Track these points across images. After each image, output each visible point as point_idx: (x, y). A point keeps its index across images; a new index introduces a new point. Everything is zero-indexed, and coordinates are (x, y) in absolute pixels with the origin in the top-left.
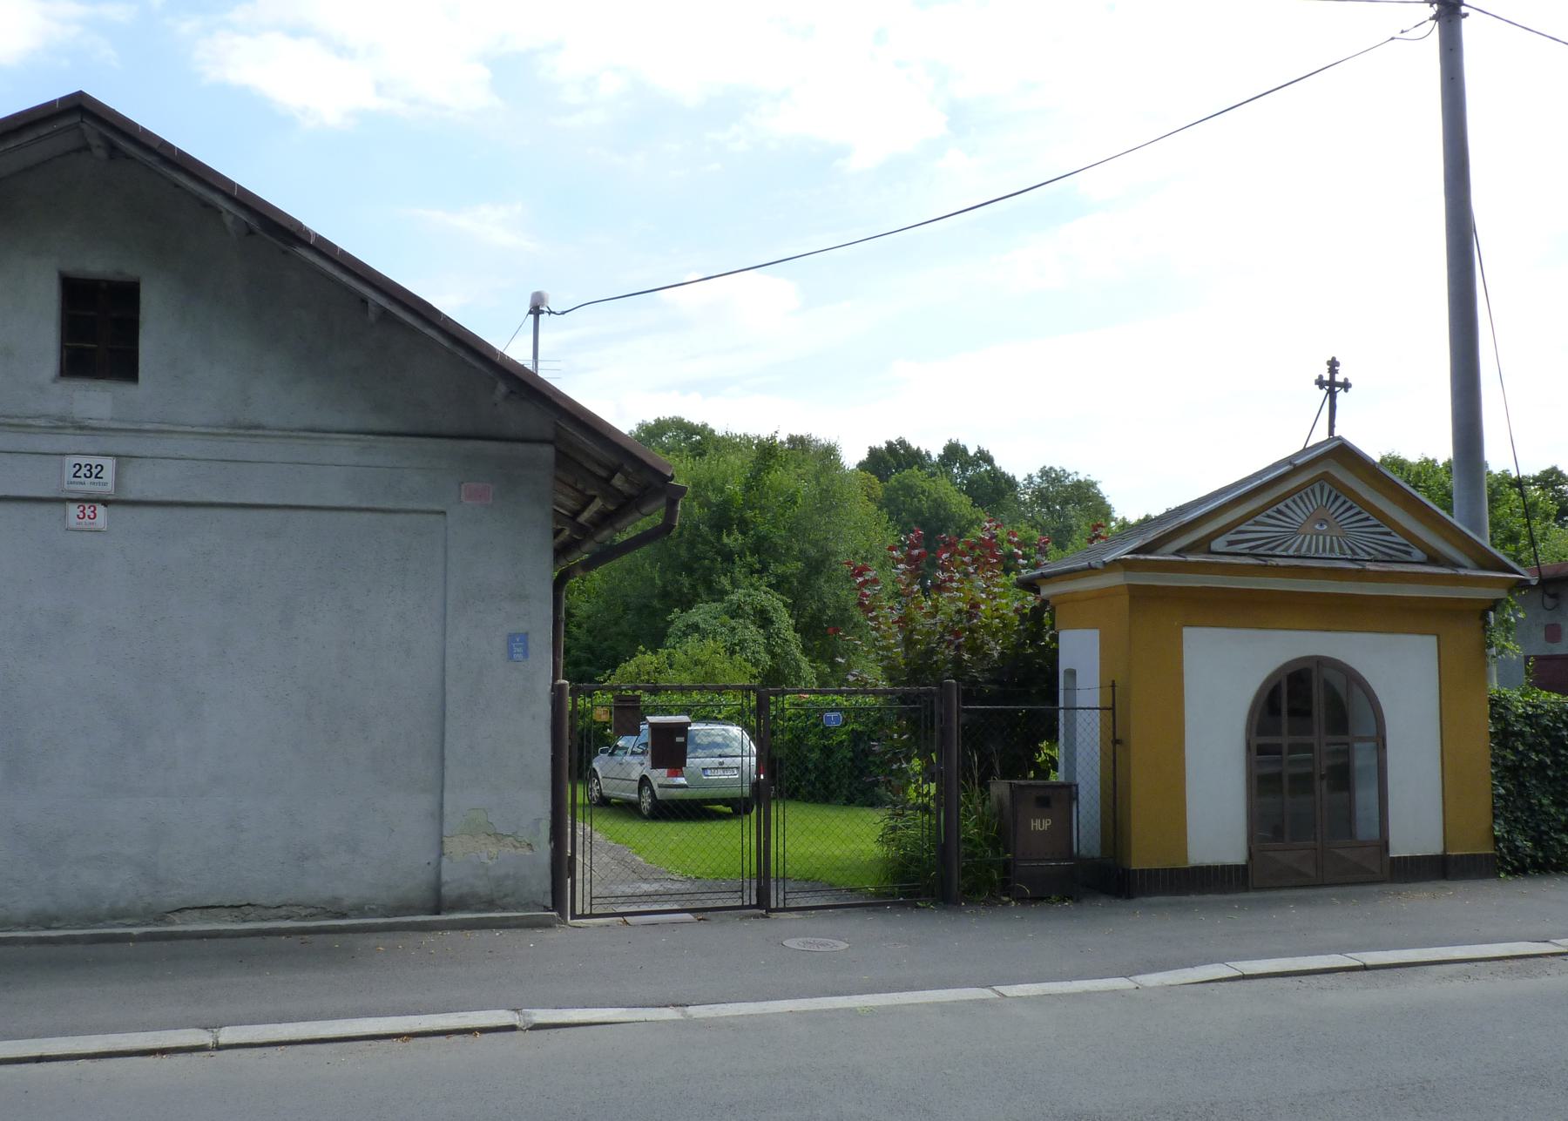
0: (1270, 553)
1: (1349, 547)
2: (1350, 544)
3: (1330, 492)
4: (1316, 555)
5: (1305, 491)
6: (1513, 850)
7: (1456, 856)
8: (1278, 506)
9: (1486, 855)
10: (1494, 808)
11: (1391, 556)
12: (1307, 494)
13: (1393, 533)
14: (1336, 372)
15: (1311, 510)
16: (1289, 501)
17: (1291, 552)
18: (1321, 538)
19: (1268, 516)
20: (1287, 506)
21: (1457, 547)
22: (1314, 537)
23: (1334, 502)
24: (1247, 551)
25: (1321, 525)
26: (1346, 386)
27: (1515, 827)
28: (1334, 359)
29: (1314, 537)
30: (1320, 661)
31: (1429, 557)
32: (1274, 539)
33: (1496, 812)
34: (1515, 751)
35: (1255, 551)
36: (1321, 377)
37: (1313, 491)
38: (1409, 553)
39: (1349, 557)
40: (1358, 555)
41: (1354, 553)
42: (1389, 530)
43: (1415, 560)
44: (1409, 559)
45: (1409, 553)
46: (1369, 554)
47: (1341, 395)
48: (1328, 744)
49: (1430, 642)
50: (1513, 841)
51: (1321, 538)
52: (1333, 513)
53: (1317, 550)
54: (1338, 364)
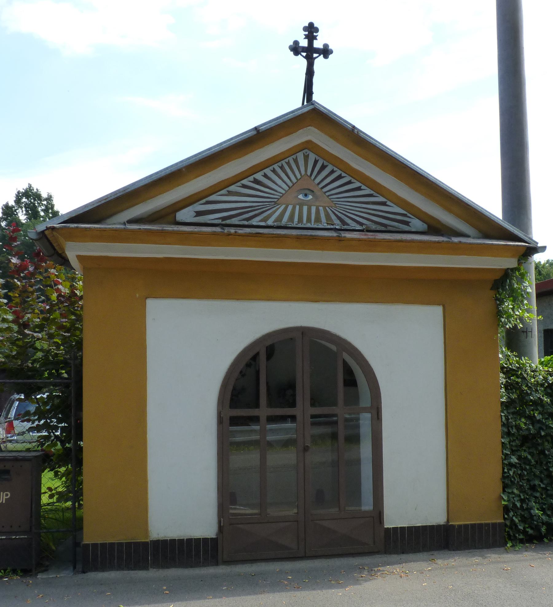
0: (246, 223)
1: (339, 218)
2: (337, 212)
3: (316, 162)
4: (300, 225)
5: (287, 160)
6: (528, 519)
7: (460, 526)
8: (255, 176)
9: (494, 525)
10: (504, 477)
11: (385, 225)
12: (288, 164)
13: (389, 203)
14: (315, 38)
15: (294, 180)
16: (268, 171)
17: (270, 222)
18: (305, 208)
19: (244, 186)
20: (265, 176)
21: (458, 216)
22: (298, 207)
23: (319, 172)
24: (219, 221)
25: (306, 195)
26: (326, 52)
27: (531, 495)
28: (311, 25)
29: (298, 207)
30: (304, 331)
31: (429, 227)
32: (252, 209)
33: (506, 481)
34: (531, 418)
35: (228, 222)
36: (296, 43)
37: (296, 161)
38: (407, 223)
39: (337, 227)
40: (348, 225)
41: (343, 222)
42: (372, 192)
43: (413, 230)
44: (406, 228)
45: (407, 223)
46: (361, 224)
47: (319, 62)
48: (313, 417)
49: (437, 311)
50: (529, 509)
51: (305, 208)
52: (319, 184)
53: (300, 220)
54: (317, 30)
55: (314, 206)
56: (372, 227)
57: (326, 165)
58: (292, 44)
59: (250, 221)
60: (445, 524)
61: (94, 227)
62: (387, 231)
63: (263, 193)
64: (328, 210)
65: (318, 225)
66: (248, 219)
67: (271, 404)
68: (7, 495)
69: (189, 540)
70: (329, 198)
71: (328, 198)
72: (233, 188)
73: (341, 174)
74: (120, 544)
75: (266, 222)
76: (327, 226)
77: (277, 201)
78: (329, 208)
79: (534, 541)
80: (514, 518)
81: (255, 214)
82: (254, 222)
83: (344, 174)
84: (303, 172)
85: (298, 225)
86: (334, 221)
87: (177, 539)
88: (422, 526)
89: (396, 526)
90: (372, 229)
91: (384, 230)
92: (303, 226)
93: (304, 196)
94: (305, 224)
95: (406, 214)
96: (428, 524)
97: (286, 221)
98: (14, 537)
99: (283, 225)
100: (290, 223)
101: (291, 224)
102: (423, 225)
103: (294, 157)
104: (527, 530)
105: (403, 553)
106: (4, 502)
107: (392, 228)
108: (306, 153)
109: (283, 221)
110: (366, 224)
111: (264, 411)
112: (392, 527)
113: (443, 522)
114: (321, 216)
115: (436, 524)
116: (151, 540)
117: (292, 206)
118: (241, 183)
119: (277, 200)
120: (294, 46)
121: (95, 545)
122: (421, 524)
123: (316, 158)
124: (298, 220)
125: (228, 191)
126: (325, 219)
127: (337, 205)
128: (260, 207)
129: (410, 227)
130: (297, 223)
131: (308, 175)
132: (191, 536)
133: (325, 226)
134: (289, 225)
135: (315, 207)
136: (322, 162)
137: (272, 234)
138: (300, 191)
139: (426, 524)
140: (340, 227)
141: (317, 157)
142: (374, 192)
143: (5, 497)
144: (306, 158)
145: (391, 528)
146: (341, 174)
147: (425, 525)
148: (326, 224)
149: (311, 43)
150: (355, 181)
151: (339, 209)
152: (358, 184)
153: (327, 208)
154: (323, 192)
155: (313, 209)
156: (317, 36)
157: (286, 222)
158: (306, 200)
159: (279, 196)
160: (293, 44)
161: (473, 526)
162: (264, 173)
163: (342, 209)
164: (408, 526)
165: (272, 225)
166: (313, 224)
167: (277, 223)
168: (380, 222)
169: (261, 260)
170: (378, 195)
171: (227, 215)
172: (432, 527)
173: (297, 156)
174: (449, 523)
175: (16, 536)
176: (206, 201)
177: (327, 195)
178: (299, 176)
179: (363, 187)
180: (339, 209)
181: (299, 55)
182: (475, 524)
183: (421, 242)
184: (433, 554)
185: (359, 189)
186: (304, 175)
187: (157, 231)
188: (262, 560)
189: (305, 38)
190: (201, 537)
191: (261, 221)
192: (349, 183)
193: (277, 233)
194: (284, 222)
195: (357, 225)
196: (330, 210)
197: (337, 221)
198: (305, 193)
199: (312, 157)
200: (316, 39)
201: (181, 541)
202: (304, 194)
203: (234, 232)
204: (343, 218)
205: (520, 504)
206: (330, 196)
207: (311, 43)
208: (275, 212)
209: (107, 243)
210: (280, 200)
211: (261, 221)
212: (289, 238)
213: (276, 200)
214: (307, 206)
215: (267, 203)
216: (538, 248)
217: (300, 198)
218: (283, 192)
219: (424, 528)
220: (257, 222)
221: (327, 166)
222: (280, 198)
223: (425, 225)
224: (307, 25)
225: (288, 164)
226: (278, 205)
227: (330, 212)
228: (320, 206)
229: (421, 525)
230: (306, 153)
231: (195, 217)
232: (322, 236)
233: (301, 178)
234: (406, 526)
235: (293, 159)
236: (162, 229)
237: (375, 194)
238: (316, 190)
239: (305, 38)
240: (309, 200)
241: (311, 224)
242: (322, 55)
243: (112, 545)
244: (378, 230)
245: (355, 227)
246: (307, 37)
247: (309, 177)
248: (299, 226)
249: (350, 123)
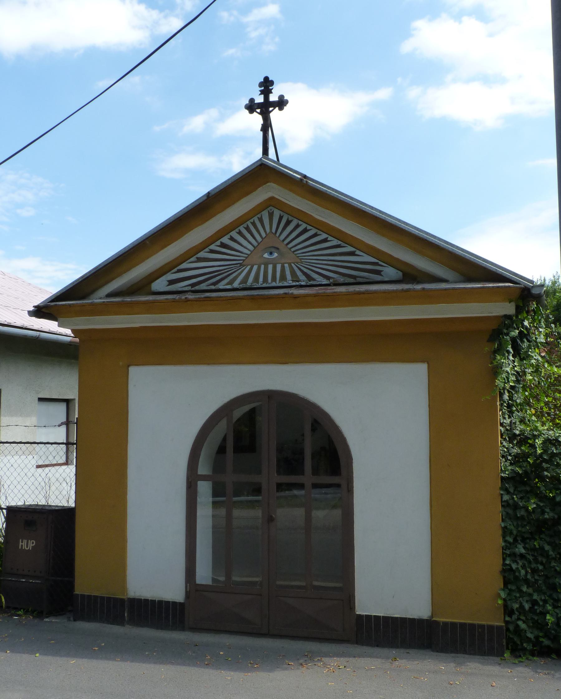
0: (213, 287)
3: (281, 218)
4: (265, 285)
5: (252, 220)
7: (446, 624)
9: (491, 627)
10: (503, 571)
11: (354, 277)
12: (254, 224)
13: (358, 252)
15: (259, 239)
16: (234, 234)
17: (236, 285)
18: (270, 267)
19: (212, 251)
20: (232, 239)
22: (263, 267)
25: (271, 253)
28: (266, 79)
29: (263, 267)
31: (405, 274)
35: (197, 288)
36: (252, 100)
37: (261, 220)
38: (378, 273)
39: (303, 283)
40: (314, 280)
42: (340, 242)
43: (386, 279)
45: (378, 273)
46: (328, 278)
47: (275, 115)
49: (421, 369)
51: (270, 267)
52: (283, 240)
53: (265, 280)
55: (280, 263)
56: (340, 280)
57: (290, 221)
58: (248, 103)
59: (217, 285)
60: (428, 619)
61: (69, 303)
62: (356, 282)
63: (229, 256)
64: (293, 266)
65: (283, 283)
66: (214, 284)
67: (315, 472)
68: (33, 543)
69: (160, 602)
70: (295, 254)
71: (294, 253)
72: (202, 254)
73: (306, 228)
74: (102, 598)
75: (232, 285)
76: (293, 283)
77: (243, 262)
78: (295, 264)
79: (552, 655)
80: (520, 623)
81: (221, 278)
82: (221, 286)
83: (309, 227)
84: (268, 230)
85: (263, 284)
86: (299, 277)
87: (143, 598)
88: (400, 617)
89: (370, 614)
90: (340, 282)
91: (353, 282)
92: (267, 285)
93: (270, 255)
94: (270, 284)
95: (378, 263)
96: (408, 617)
97: (251, 282)
98: (31, 581)
99: (248, 287)
100: (255, 284)
101: (256, 285)
102: (397, 273)
103: (259, 216)
104: (541, 639)
105: (377, 646)
106: (31, 549)
107: (362, 279)
108: (271, 210)
109: (248, 282)
110: (333, 277)
111: (308, 478)
112: (364, 614)
113: (427, 616)
114: (286, 273)
115: (417, 618)
116: (128, 597)
117: (257, 266)
118: (208, 249)
119: (243, 261)
120: (250, 104)
121: (83, 596)
122: (400, 615)
123: (280, 214)
124: (263, 280)
125: (197, 258)
126: (290, 276)
127: (302, 260)
128: (226, 271)
129: (382, 276)
130: (262, 283)
131: (273, 233)
132: (162, 598)
133: (290, 283)
134: (254, 285)
135: (281, 264)
136: (287, 217)
137: (200, 298)
138: (265, 250)
139: (405, 616)
140: (306, 283)
141: (282, 213)
142: (341, 242)
143: (31, 545)
144: (271, 215)
145: (363, 615)
146: (306, 227)
147: (405, 617)
148: (291, 282)
149: (266, 98)
150: (321, 233)
151: (304, 264)
152: (324, 236)
153: (293, 265)
154: (288, 248)
155: (279, 267)
156: (272, 89)
157: (251, 283)
158: (271, 258)
159: (245, 257)
160: (249, 102)
161: (463, 625)
162: (230, 235)
163: (307, 263)
164: (383, 615)
165: (237, 287)
166: (278, 282)
167: (242, 285)
168: (348, 273)
169: (225, 324)
170: (347, 245)
171: (197, 281)
172: (412, 621)
173: (261, 215)
174: (433, 618)
175: (32, 581)
176: (177, 270)
177: (292, 251)
178: (264, 235)
179: (330, 238)
180: (304, 264)
181: (255, 112)
182: (465, 624)
183: (385, 292)
184: (408, 653)
185: (325, 240)
186: (269, 233)
187: (118, 303)
188: (226, 631)
189: (260, 94)
190: (171, 601)
191: (227, 284)
192: (315, 235)
193: (224, 296)
194: (249, 283)
195: (324, 280)
196: (295, 266)
197: (302, 277)
198: (270, 251)
199: (277, 214)
200: (272, 93)
201: (153, 602)
202: (269, 253)
203: (184, 298)
204: (308, 273)
205: (531, 606)
206: (295, 252)
207: (266, 98)
208: (240, 274)
209: (89, 317)
210: (245, 261)
211: (227, 284)
212: (244, 299)
213: (241, 262)
214: (272, 265)
215: (233, 266)
216: (530, 288)
217: (265, 257)
218: (249, 252)
219: (403, 621)
220: (224, 286)
221: (292, 221)
222: (246, 259)
223: (399, 272)
224: (263, 81)
225: (254, 224)
226: (244, 266)
227: (295, 268)
228: (286, 263)
229: (399, 616)
230: (271, 210)
231: (168, 285)
232: (275, 295)
233: (265, 237)
234: (382, 615)
235: (258, 218)
236: (122, 300)
237: (343, 244)
238: (282, 246)
239: (260, 94)
240: (275, 258)
241: (276, 283)
242: (277, 108)
243: (96, 597)
244: (346, 283)
245: (321, 281)
246: (262, 92)
247: (274, 234)
248: (264, 285)
249: (301, 173)
